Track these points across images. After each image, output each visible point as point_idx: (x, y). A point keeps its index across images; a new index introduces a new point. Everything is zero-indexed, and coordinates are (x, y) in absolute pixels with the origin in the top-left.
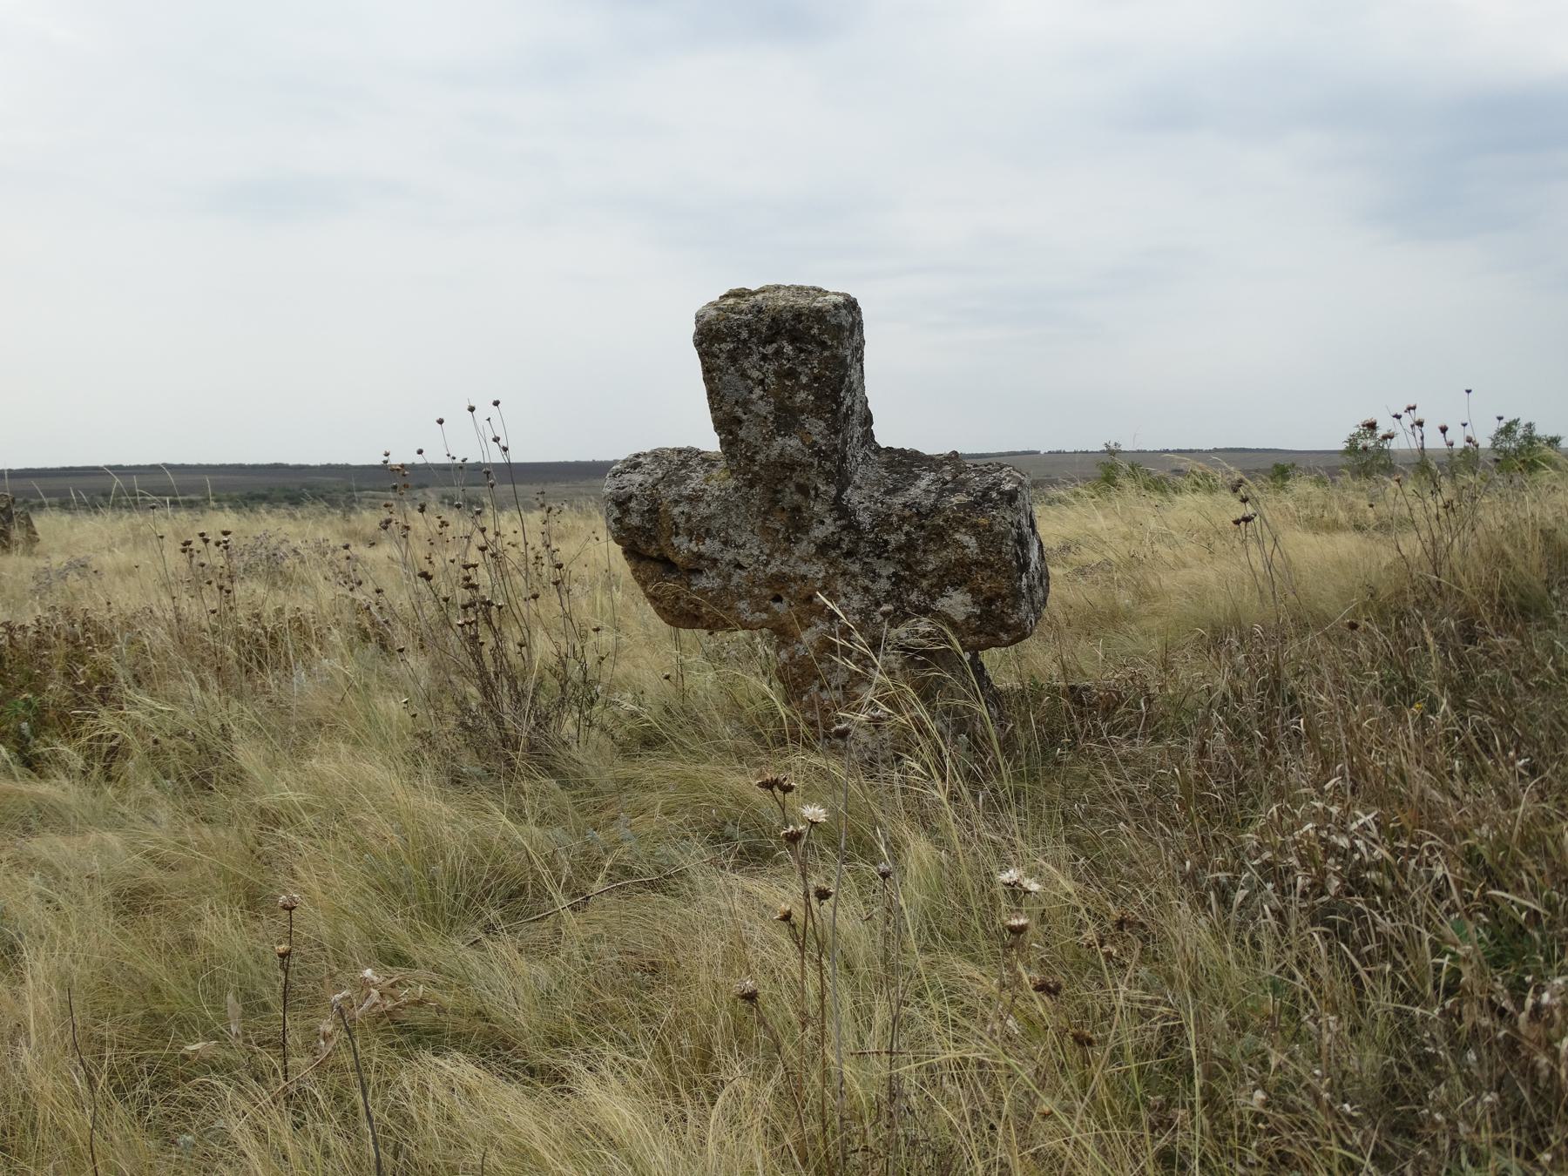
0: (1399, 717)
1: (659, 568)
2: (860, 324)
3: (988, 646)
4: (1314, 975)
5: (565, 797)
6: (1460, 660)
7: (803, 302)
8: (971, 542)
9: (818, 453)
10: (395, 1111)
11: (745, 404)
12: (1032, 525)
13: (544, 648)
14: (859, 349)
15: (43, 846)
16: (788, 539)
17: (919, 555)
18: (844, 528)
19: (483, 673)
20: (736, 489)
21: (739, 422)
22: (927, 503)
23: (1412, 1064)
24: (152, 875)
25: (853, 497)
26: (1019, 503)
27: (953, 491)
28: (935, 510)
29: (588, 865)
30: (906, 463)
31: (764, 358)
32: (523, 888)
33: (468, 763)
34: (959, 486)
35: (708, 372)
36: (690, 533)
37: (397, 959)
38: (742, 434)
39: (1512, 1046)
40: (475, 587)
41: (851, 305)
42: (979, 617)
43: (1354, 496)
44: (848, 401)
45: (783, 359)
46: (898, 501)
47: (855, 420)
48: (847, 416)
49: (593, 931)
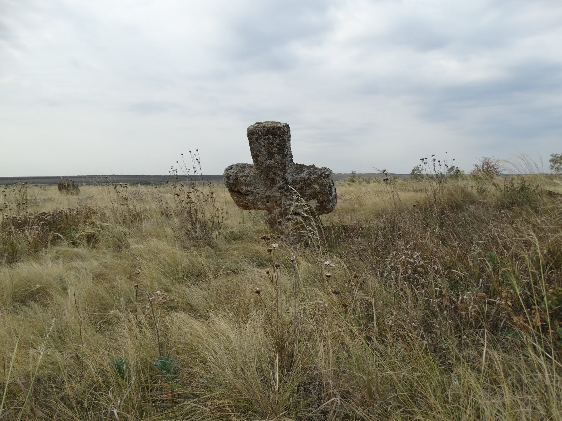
0: (426, 231)
1: (238, 194)
2: (290, 131)
3: (322, 214)
4: (405, 293)
5: (213, 251)
6: (441, 219)
7: (275, 125)
8: (317, 187)
9: (278, 164)
10: (165, 326)
11: (260, 151)
12: (333, 183)
13: (208, 215)
14: (289, 137)
15: (78, 264)
16: (271, 186)
17: (304, 190)
18: (285, 183)
19: (192, 220)
20: (258, 173)
21: (259, 156)
22: (306, 177)
23: (430, 315)
24: (104, 270)
25: (287, 176)
26: (330, 177)
27: (313, 174)
28: (308, 179)
29: (218, 269)
30: (301, 167)
31: (265, 139)
32: (201, 273)
33: (188, 244)
34: (315, 173)
35: (251, 143)
36: (246, 185)
37: (168, 290)
38: (259, 159)
39: (456, 308)
40: (190, 198)
41: (287, 126)
42: (319, 206)
43: (414, 184)
44: (286, 151)
45: (270, 140)
46: (299, 176)
47: (288, 156)
48: (286, 155)
49: (218, 284)
